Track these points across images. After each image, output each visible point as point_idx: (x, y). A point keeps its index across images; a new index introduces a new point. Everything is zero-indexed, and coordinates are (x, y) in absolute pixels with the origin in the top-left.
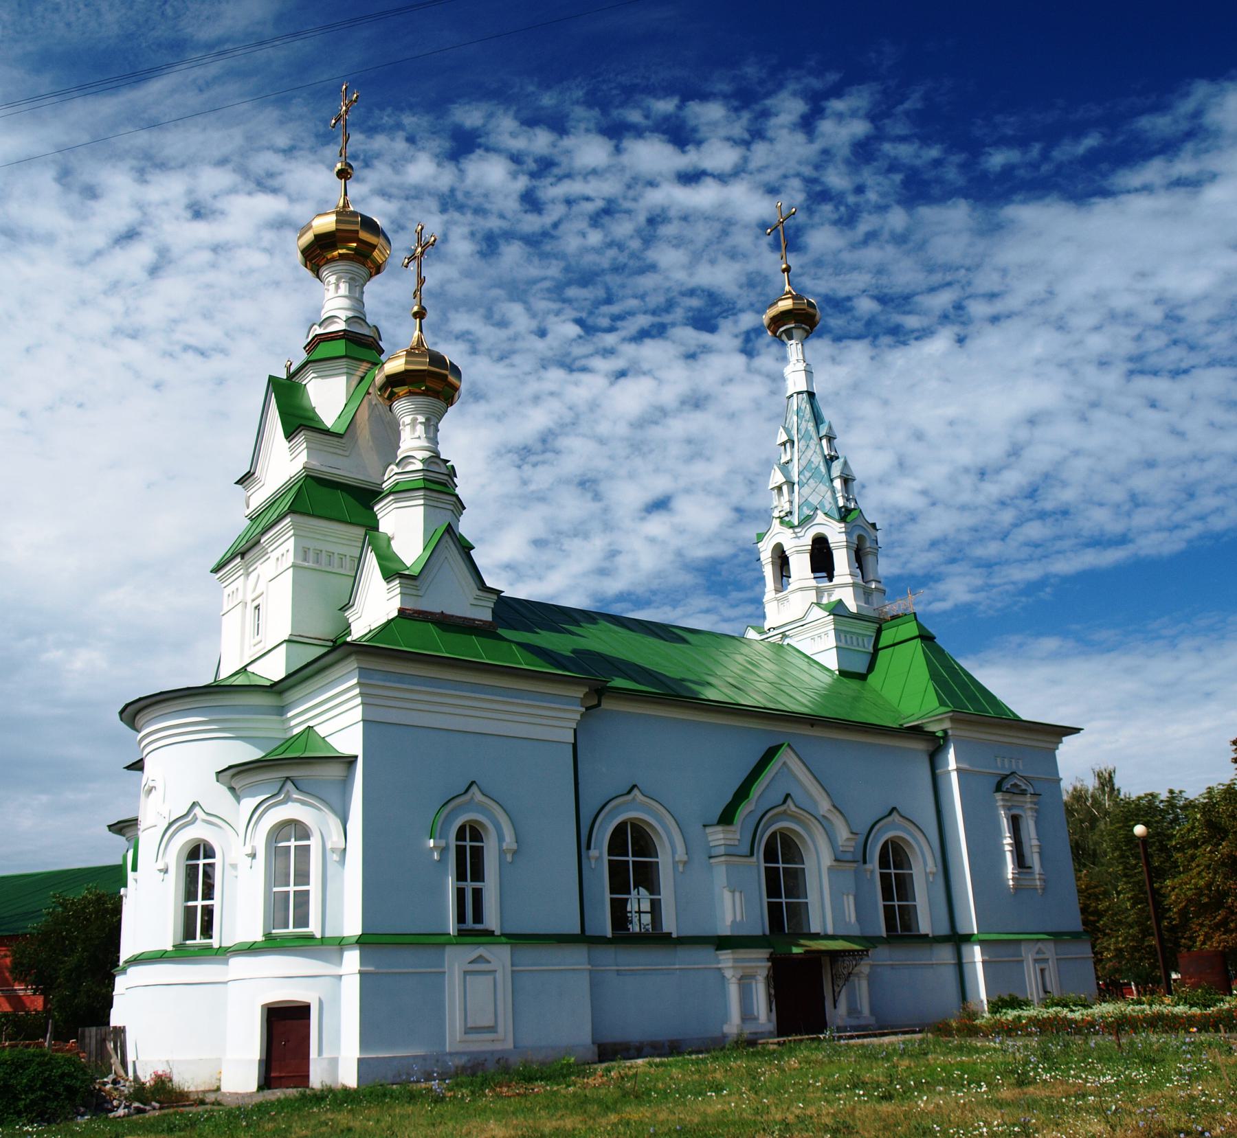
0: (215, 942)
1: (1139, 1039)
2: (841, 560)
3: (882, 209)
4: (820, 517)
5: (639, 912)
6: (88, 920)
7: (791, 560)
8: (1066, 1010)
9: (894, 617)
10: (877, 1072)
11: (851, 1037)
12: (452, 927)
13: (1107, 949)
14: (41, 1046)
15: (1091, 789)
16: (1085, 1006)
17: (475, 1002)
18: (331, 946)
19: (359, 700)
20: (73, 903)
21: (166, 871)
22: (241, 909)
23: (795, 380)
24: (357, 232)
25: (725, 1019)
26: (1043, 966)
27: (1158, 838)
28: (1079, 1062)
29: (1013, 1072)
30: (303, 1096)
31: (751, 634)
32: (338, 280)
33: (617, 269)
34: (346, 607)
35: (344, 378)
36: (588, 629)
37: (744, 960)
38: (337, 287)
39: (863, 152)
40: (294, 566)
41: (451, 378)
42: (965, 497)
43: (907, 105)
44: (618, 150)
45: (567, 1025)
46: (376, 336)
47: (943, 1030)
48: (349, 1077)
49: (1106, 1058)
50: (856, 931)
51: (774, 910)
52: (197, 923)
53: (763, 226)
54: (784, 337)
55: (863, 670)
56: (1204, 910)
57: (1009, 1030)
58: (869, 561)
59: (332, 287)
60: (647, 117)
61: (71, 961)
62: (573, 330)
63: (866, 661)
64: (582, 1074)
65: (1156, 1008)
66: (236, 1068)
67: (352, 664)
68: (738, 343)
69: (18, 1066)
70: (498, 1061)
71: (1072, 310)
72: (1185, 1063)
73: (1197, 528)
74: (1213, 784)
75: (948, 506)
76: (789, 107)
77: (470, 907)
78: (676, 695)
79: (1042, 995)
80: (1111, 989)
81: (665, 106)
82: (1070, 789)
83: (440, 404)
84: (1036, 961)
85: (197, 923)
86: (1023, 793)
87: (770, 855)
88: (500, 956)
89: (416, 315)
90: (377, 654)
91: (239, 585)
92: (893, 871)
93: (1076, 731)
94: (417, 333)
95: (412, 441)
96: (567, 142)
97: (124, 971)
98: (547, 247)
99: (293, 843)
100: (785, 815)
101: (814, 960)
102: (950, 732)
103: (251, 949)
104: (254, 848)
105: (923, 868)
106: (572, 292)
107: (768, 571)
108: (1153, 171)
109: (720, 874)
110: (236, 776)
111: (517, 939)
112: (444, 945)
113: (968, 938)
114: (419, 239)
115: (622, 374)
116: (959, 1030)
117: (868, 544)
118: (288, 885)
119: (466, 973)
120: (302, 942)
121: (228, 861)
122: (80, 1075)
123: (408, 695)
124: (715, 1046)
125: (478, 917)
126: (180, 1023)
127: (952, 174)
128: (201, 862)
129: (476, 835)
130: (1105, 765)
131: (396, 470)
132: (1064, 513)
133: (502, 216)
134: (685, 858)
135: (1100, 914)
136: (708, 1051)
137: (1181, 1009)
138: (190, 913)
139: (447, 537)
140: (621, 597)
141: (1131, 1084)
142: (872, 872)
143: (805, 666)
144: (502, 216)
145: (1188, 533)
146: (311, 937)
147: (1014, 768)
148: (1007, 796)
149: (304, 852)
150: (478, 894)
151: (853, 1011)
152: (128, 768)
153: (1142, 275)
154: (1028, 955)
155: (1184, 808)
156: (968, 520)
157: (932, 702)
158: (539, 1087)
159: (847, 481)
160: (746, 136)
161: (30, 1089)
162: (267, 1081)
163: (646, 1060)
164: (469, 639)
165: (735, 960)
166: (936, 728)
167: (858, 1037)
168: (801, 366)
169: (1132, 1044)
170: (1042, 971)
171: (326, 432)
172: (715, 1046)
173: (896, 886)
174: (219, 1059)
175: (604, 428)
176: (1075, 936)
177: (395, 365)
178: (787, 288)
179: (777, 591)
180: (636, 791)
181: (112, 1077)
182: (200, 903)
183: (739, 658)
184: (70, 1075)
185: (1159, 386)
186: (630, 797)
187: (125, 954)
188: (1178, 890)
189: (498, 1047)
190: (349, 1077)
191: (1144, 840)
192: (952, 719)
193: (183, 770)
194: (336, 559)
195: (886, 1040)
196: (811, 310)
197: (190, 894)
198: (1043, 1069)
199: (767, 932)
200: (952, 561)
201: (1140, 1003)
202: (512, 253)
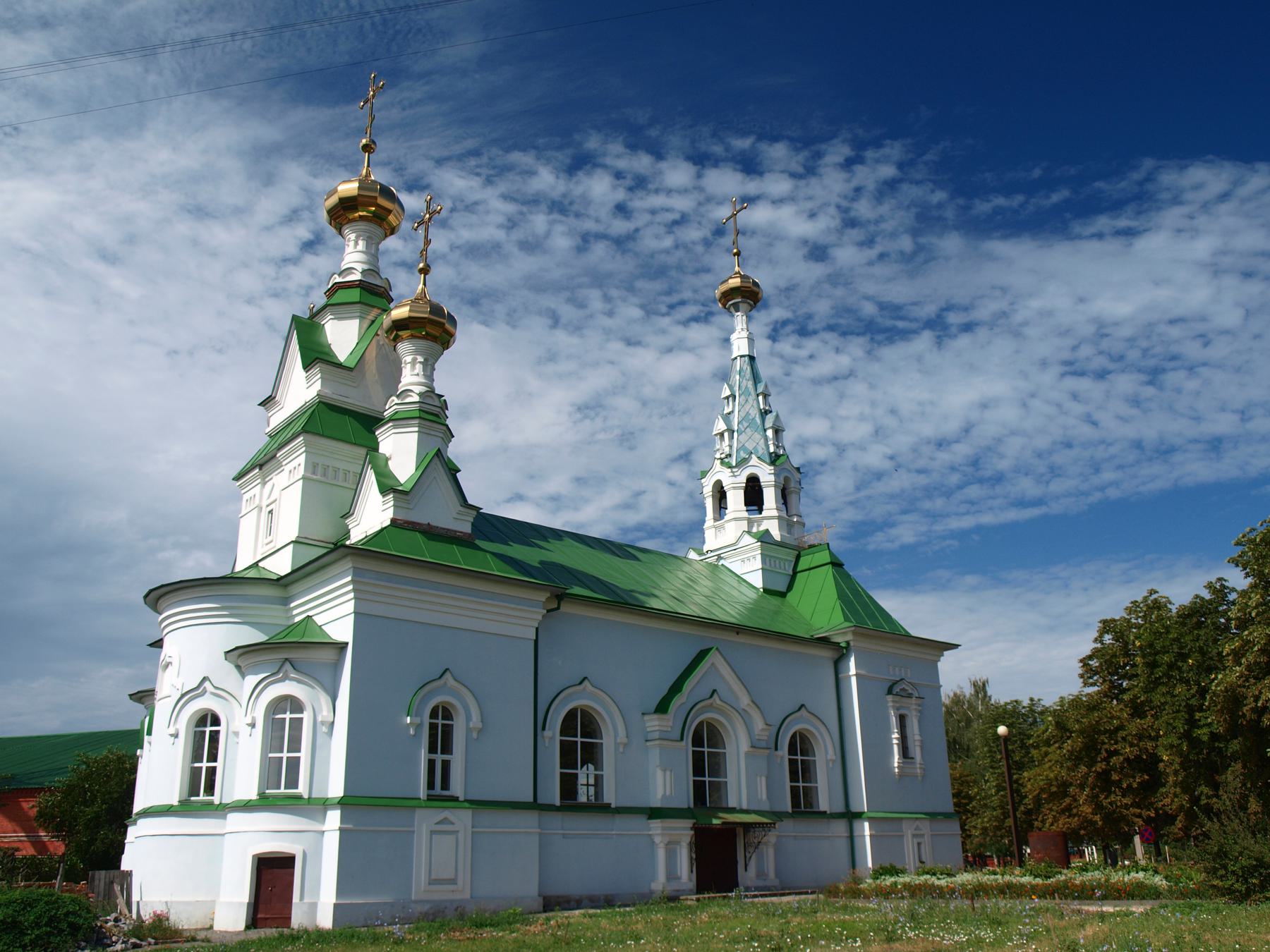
0: (216, 799)
1: (990, 903)
2: (770, 497)
3: (893, 235)
4: (754, 460)
5: (588, 785)
6: (108, 776)
7: (729, 495)
8: (934, 878)
9: (811, 546)
10: (771, 928)
11: (755, 896)
12: (422, 792)
13: (975, 827)
14: (53, 886)
15: (968, 695)
16: (950, 875)
17: (440, 856)
18: (314, 807)
19: (352, 595)
20: (96, 761)
21: (176, 736)
22: (241, 771)
23: (740, 346)
24: (376, 198)
25: (653, 877)
27: (1019, 737)
28: (939, 922)
29: (883, 930)
30: (281, 935)
31: (692, 555)
32: (357, 238)
33: (680, 268)
34: (347, 515)
35: (357, 321)
36: (554, 545)
37: (671, 828)
38: (356, 244)
39: (889, 187)
40: (304, 478)
41: (448, 326)
42: (921, 463)
43: (928, 157)
44: (699, 176)
45: (519, 879)
46: (387, 287)
47: (833, 892)
48: (325, 920)
49: (961, 920)
50: (766, 808)
51: (699, 788)
53: (805, 242)
54: (732, 309)
55: (783, 589)
56: (1053, 797)
57: (886, 893)
58: (792, 499)
59: (352, 244)
60: (727, 150)
61: (90, 811)
62: (636, 313)
63: (787, 580)
64: (527, 923)
65: (1007, 878)
66: (230, 909)
67: (347, 564)
68: (767, 330)
69: (27, 904)
70: (456, 910)
71: (1025, 323)
72: (1025, 924)
73: (1098, 496)
74: (1065, 694)
75: (909, 470)
76: (838, 152)
77: (439, 776)
78: (624, 602)
79: (918, 864)
80: (976, 861)
81: (742, 144)
82: (952, 695)
83: (438, 347)
84: (914, 836)
86: (910, 696)
87: (697, 741)
88: (463, 819)
89: (421, 271)
90: (371, 554)
91: (254, 493)
93: (956, 646)
94: (421, 286)
95: (411, 378)
96: (663, 165)
97: (135, 823)
98: (631, 245)
99: (288, 716)
100: (711, 707)
101: (730, 831)
102: (852, 644)
103: (246, 807)
104: (254, 718)
105: (824, 756)
106: (639, 284)
107: (709, 503)
108: (1103, 222)
109: (655, 756)
110: (242, 656)
111: (477, 804)
112: (414, 807)
113: (859, 815)
114: (428, 207)
115: (669, 350)
116: (845, 893)
117: (792, 485)
118: (282, 751)
119: (433, 832)
120: (292, 802)
121: (232, 729)
122: (84, 914)
123: (453, 603)
124: (643, 900)
125: (446, 785)
126: (179, 868)
127: (950, 213)
128: (208, 729)
129: (448, 715)
130: (980, 676)
131: (396, 401)
132: (999, 478)
133: (597, 220)
134: (625, 740)
135: (971, 799)
136: (634, 905)
137: (1027, 879)
138: (195, 773)
139: (436, 460)
140: (639, 527)
141: (980, 941)
142: (782, 757)
143: (735, 584)
144: (597, 220)
145: (1091, 499)
146: (300, 797)
147: (903, 676)
148: (897, 698)
149: (297, 725)
150: (446, 766)
151: (761, 874)
152: (151, 645)
153: (1082, 300)
154: (908, 831)
155: (1042, 713)
156: (922, 480)
157: (838, 618)
158: (487, 933)
159: (778, 431)
160: (801, 170)
161: (37, 925)
162: (254, 922)
163: (582, 911)
164: (451, 545)
165: (664, 829)
167: (762, 896)
168: (745, 334)
169: (984, 907)
170: (919, 844)
171: (339, 365)
172: (643, 900)
173: (801, 770)
174: (214, 901)
175: (648, 391)
176: (947, 816)
177: (400, 312)
178: (737, 269)
179: (715, 520)
180: (586, 682)
181: (114, 915)
182: (205, 765)
183: (681, 575)
184: (74, 913)
185: (1084, 384)
187: (138, 807)
188: (1033, 780)
189: (457, 896)
190: (325, 920)
191: (1006, 739)
192: (854, 633)
193: (195, 648)
194: (330, 472)
195: (785, 899)
196: (755, 289)
197: (197, 757)
198: (910, 928)
199: (692, 805)
200: (905, 512)
201: (995, 873)
202: (600, 250)
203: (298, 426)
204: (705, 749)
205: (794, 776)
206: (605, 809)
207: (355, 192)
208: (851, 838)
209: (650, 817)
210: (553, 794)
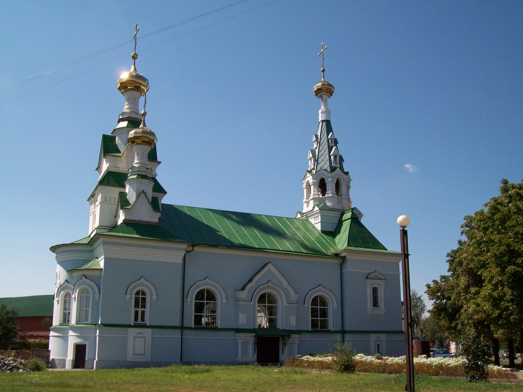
26: (379, 343)
58: (343, 188)
88: (149, 331)
105: (333, 306)
119: (135, 337)
125: (143, 319)
150: (143, 312)
186: (267, 285)
206: (216, 329)
210: (190, 322)
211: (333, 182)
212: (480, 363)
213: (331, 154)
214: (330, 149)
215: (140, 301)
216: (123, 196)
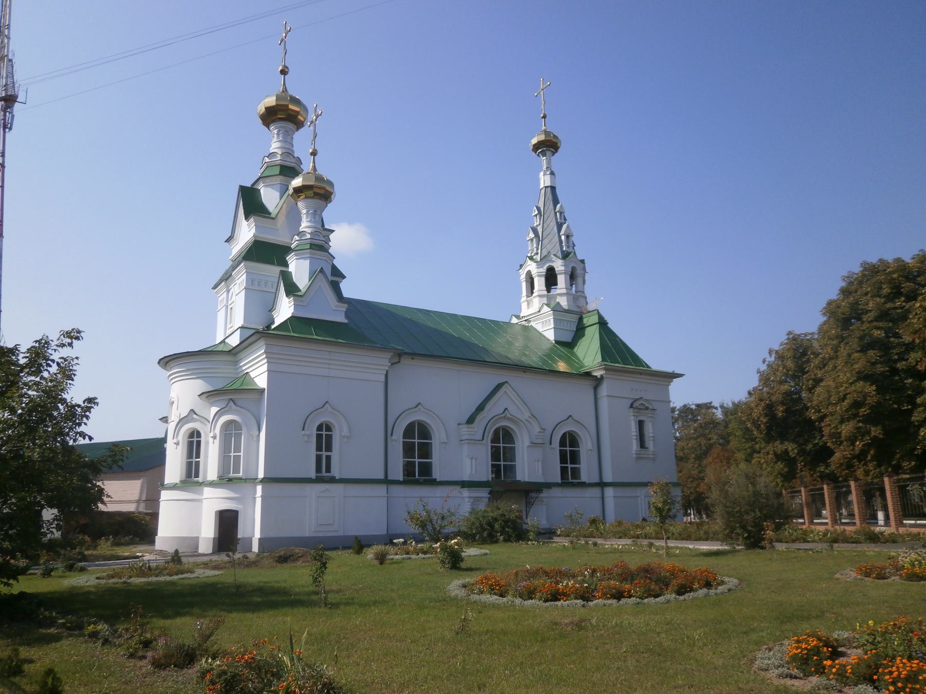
2: (561, 280)
17: (317, 512)
22: (211, 466)
32: (279, 131)
34: (271, 310)
52: (192, 471)
83: (322, 203)
85: (192, 471)
92: (568, 449)
93: (680, 375)
105: (586, 447)
125: (328, 470)
150: (328, 458)
166: (598, 374)
179: (528, 296)
182: (194, 460)
192: (606, 369)
196: (554, 140)
203: (240, 258)
204: (502, 443)
205: (563, 459)
207: (274, 104)
208: (603, 498)
209: (463, 487)
210: (397, 473)
211: (566, 271)
212: (48, 514)
213: (562, 232)
214: (559, 227)
215: (324, 439)
216: (286, 278)
